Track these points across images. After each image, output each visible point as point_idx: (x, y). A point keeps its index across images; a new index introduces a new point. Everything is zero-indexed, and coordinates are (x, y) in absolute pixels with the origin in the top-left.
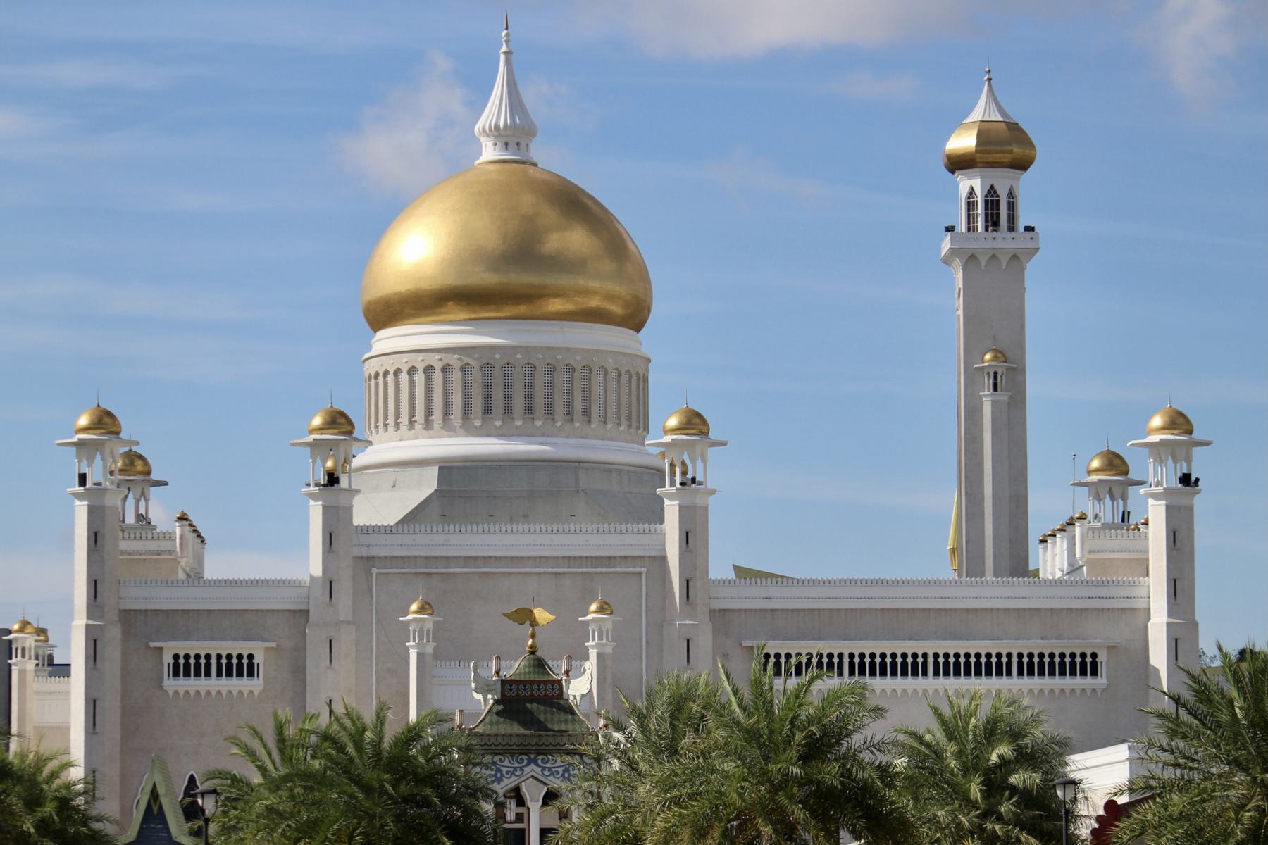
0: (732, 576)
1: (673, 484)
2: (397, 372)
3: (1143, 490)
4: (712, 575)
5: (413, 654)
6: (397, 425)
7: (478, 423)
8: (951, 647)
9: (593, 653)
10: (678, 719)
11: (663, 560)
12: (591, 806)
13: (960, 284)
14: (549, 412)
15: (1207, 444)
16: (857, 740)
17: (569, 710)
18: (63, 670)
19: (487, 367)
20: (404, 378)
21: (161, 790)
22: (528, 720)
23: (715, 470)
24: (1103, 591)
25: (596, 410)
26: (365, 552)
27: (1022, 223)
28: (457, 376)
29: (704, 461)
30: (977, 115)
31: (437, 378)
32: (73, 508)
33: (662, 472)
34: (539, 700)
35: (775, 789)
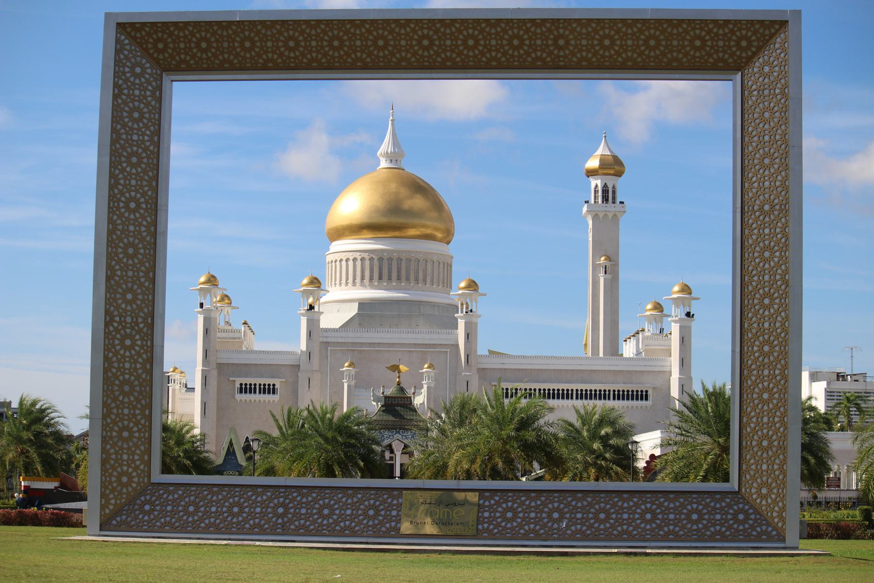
0: (487, 353)
1: (462, 312)
2: (341, 261)
3: (669, 319)
4: (479, 352)
5: (346, 385)
6: (340, 284)
7: (376, 284)
8: (584, 387)
9: (425, 386)
10: (464, 412)
11: (457, 346)
12: (424, 451)
13: (591, 226)
14: (408, 279)
15: (698, 299)
16: (541, 422)
17: (415, 410)
18: (192, 390)
19: (381, 259)
20: (344, 263)
21: (234, 442)
22: (396, 414)
23: (481, 306)
24: (651, 363)
25: (428, 279)
26: (325, 340)
27: (618, 200)
28: (367, 263)
29: (476, 302)
30: (600, 152)
31: (359, 263)
32: (197, 318)
33: (457, 307)
34: (401, 406)
35: (505, 443)
